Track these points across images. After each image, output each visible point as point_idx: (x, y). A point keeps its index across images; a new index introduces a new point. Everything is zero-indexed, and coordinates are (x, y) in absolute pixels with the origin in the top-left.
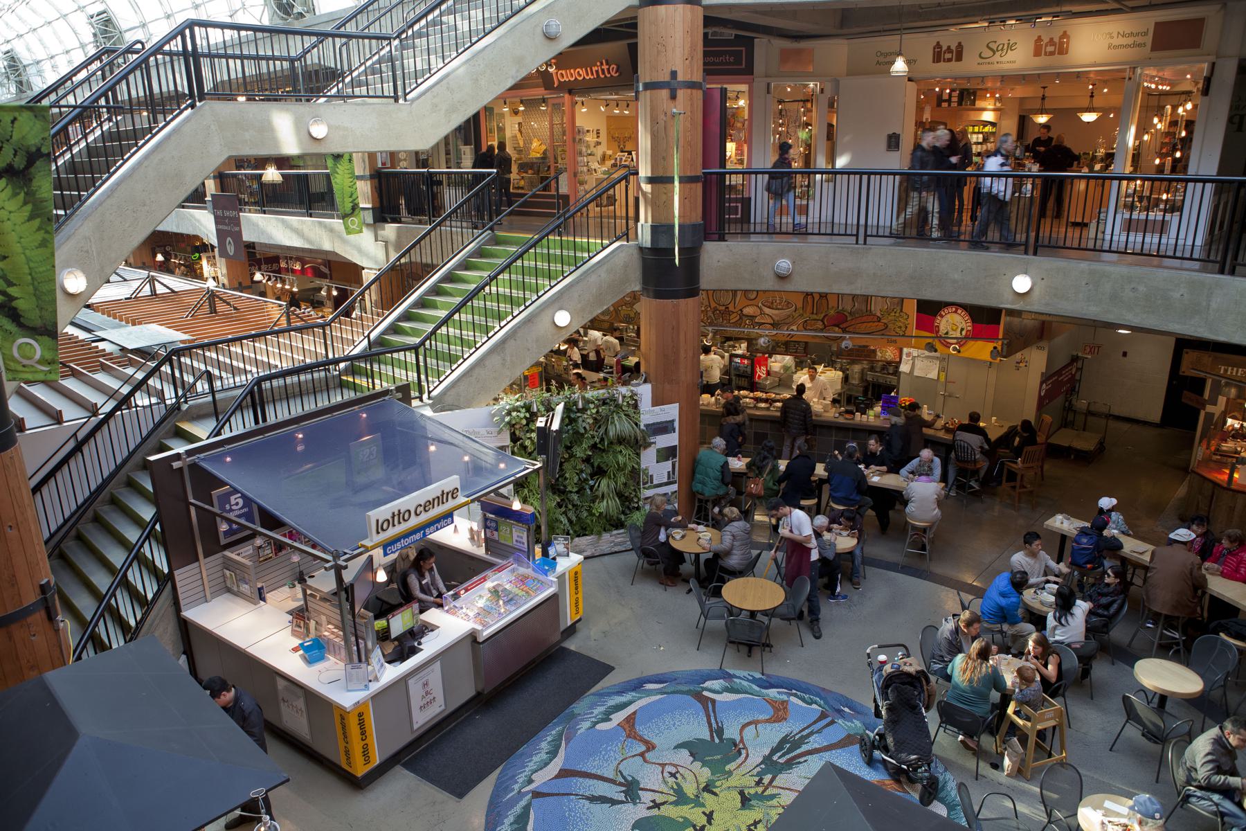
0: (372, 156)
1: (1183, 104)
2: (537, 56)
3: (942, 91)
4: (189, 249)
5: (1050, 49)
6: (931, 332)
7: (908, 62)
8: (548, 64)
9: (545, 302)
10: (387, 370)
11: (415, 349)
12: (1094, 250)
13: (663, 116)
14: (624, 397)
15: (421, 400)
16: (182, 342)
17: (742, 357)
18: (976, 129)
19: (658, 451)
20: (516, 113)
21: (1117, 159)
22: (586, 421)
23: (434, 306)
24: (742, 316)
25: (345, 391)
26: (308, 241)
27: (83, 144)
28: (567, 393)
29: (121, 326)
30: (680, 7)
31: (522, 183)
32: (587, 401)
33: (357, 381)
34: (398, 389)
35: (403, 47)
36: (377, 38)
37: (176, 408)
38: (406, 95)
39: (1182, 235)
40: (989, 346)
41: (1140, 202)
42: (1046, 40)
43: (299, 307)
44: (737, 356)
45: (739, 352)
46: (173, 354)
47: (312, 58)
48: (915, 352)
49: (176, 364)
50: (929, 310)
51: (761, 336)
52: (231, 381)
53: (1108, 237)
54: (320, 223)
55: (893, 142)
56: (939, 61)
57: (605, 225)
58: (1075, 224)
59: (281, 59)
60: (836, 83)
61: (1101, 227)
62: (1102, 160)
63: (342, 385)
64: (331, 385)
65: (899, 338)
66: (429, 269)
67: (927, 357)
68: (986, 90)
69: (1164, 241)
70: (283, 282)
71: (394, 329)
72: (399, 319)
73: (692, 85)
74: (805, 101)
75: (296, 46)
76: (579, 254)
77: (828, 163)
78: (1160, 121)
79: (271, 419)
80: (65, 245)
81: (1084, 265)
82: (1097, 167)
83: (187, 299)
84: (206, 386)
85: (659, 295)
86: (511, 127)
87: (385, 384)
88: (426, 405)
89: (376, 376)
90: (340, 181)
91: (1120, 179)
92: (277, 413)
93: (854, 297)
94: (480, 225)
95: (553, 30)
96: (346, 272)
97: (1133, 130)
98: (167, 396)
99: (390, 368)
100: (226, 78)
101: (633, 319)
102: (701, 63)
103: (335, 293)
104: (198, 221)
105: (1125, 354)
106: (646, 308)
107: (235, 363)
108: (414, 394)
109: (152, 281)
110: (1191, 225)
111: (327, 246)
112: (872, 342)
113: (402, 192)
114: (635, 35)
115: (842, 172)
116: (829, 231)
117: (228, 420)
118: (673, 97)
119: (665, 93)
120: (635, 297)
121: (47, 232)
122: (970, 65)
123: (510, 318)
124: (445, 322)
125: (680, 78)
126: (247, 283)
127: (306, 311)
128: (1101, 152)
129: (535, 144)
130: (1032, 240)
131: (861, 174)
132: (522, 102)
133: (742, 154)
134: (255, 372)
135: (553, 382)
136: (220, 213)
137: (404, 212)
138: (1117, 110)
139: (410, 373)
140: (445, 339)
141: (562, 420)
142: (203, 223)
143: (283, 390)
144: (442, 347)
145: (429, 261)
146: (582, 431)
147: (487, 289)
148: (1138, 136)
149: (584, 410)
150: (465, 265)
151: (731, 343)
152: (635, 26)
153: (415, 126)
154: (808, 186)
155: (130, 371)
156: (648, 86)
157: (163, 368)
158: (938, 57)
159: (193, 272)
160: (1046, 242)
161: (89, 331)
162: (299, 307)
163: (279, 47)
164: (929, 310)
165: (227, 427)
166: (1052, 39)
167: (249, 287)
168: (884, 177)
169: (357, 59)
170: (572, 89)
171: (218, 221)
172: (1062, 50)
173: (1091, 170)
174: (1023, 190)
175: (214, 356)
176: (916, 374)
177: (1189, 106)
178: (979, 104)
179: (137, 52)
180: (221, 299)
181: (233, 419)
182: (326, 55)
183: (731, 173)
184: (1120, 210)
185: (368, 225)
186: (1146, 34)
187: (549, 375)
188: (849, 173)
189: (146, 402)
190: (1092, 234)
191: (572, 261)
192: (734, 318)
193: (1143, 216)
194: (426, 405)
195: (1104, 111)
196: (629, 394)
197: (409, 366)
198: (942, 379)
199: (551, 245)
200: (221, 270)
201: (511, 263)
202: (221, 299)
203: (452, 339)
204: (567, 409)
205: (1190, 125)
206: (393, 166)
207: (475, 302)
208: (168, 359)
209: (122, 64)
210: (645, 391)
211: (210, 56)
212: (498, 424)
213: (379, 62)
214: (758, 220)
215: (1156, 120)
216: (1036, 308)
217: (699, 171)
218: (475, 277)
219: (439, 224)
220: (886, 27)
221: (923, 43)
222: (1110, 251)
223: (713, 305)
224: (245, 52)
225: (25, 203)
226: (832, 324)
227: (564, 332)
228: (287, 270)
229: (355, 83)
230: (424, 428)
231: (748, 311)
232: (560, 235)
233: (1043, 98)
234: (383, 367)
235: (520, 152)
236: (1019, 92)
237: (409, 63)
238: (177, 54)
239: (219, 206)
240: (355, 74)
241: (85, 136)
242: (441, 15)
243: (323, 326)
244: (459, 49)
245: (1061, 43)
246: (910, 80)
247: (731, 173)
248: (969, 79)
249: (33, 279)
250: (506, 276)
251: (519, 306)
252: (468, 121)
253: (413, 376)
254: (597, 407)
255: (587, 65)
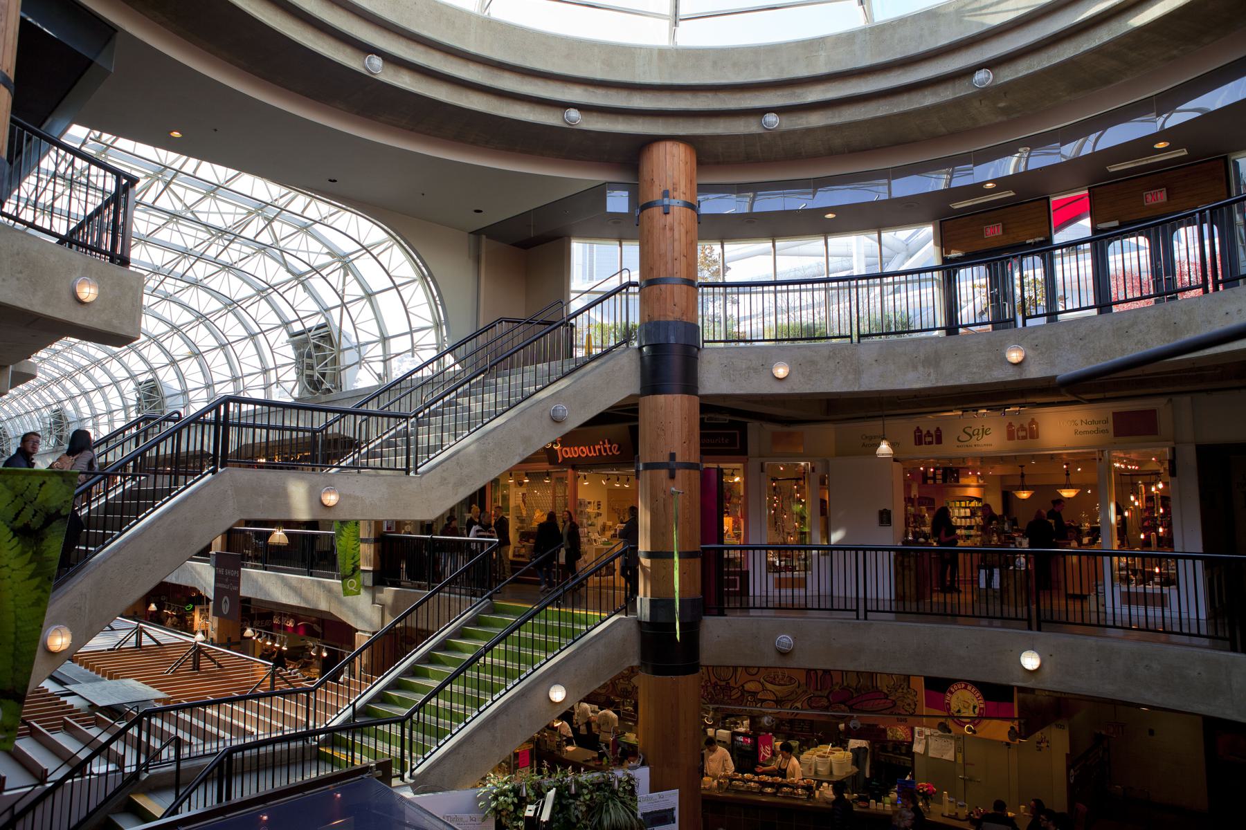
0: (378, 523)
1: (1155, 483)
2: (546, 437)
3: (926, 469)
4: (184, 599)
5: (1022, 434)
6: (942, 709)
7: (892, 445)
8: (555, 443)
9: (541, 675)
10: (369, 742)
11: (401, 721)
12: (1098, 625)
13: (662, 495)
14: (620, 781)
15: (402, 779)
16: (157, 700)
17: (745, 735)
18: (963, 504)
20: (521, 484)
21: (1103, 532)
22: (578, 809)
23: (425, 675)
24: (743, 691)
25: (322, 765)
26: (305, 600)
27: (103, 501)
28: (559, 776)
29: (96, 680)
30: (678, 397)
31: (523, 551)
32: (580, 786)
33: (336, 754)
34: (379, 766)
35: (419, 423)
36: (396, 417)
37: (135, 776)
38: (417, 468)
39: (1184, 609)
40: (1007, 726)
41: (1135, 575)
42: (1016, 426)
43: (285, 667)
44: (740, 734)
45: (742, 730)
46: (142, 716)
47: (334, 429)
48: (927, 732)
49: (145, 725)
50: (938, 686)
51: (765, 714)
52: (201, 748)
53: (1110, 610)
54: (319, 582)
55: (885, 518)
56: (920, 443)
57: (604, 596)
58: (1074, 597)
59: (304, 430)
60: (827, 464)
61: (1101, 600)
62: (1088, 534)
63: (320, 758)
64: (308, 757)
65: (910, 717)
66: (425, 635)
67: (940, 736)
68: (968, 468)
69: (1167, 614)
70: (273, 639)
71: (381, 698)
72: (388, 687)
73: (689, 466)
74: (798, 479)
75: (319, 420)
76: (577, 627)
77: (823, 537)
78: (1137, 499)
79: (236, 797)
80: (60, 602)
81: (1091, 641)
82: (1086, 540)
83: (171, 653)
84: (172, 753)
85: (657, 671)
86: (515, 497)
87: (365, 759)
88: (408, 784)
89: (357, 748)
90: (344, 544)
91: (1111, 555)
92: (245, 789)
93: (859, 674)
94: (479, 593)
95: (560, 413)
96: (336, 632)
97: (1113, 507)
98: (127, 762)
99: (372, 740)
100: (250, 441)
101: (630, 694)
102: (698, 446)
103: (325, 654)
104: (199, 574)
105: (1151, 732)
106: (645, 683)
107: (208, 727)
108: (396, 771)
109: (139, 632)
110: (1190, 599)
111: (323, 606)
112: (880, 721)
113: (403, 556)
114: (636, 419)
115: (837, 548)
116: (829, 606)
117: (189, 796)
118: (672, 477)
119: (664, 473)
120: (632, 670)
121: (45, 591)
122: (950, 448)
123: (503, 691)
124: (436, 693)
125: (679, 459)
126: (236, 638)
127: (292, 671)
128: (1086, 526)
129: (538, 514)
130: (1034, 614)
131: (857, 550)
132: (527, 475)
133: (739, 529)
134: (229, 740)
135: (545, 763)
136: (221, 571)
137: (404, 576)
138: (1094, 487)
139: (393, 747)
140: (434, 711)
141: (554, 806)
142: (204, 576)
143: (254, 761)
144: (430, 719)
145: (425, 627)
146: (574, 820)
147: (481, 660)
148: (1119, 511)
149: (576, 796)
150: (461, 633)
151: (733, 719)
152: (636, 411)
153: (424, 499)
154: (805, 559)
155: (93, 732)
156: (648, 466)
157: (130, 731)
158: (919, 440)
159: (184, 625)
160: (1048, 617)
161: (62, 683)
162: (285, 667)
163: (304, 420)
164: (938, 686)
165: (185, 805)
166: (1022, 426)
167: (238, 643)
168: (879, 553)
169: (374, 431)
170: (576, 465)
171: (218, 578)
172: (1034, 435)
173: (1080, 544)
174: (1017, 563)
175: (188, 718)
176: (931, 754)
177: (1160, 486)
178: (963, 481)
179: (175, 421)
180: (206, 655)
181: (194, 795)
182: (348, 428)
183: (728, 549)
184: (1117, 583)
185: (366, 588)
186: (1107, 422)
187: (542, 753)
188: (845, 549)
189: (103, 769)
190: (1093, 607)
191: (570, 633)
192: (736, 694)
193: (1140, 588)
194: (408, 784)
195: (1082, 487)
196: (625, 778)
197: (393, 739)
198: (960, 760)
199: (549, 616)
200: (213, 623)
201: (508, 634)
202: (206, 655)
203: (441, 712)
204: (559, 796)
205: (1165, 500)
206: (398, 531)
207: (468, 672)
208: (137, 722)
209: (155, 434)
210: (642, 775)
211: (240, 426)
212: (483, 810)
213: (395, 436)
214: (758, 593)
215: (1132, 498)
216: (1049, 685)
217: (698, 547)
218: (470, 645)
219: (439, 590)
220: (869, 414)
221: (905, 427)
222: (1114, 627)
223: (713, 680)
224: (272, 423)
225: (30, 562)
226: (838, 701)
227: (558, 708)
228: (279, 627)
229: (371, 454)
230: (402, 813)
231: (750, 686)
232: (559, 606)
233: (1023, 476)
234: (365, 739)
235: (522, 521)
236: (998, 470)
237: (423, 438)
238: (210, 423)
239: (220, 562)
240: (371, 446)
241: (106, 494)
242: (457, 396)
243: (308, 691)
244: (471, 424)
245: (1031, 429)
246: (895, 460)
247: (728, 549)
248: (950, 460)
249: (17, 638)
250: (502, 646)
251: (514, 679)
252: (475, 494)
253: (396, 750)
254: (591, 792)
255: (590, 443)
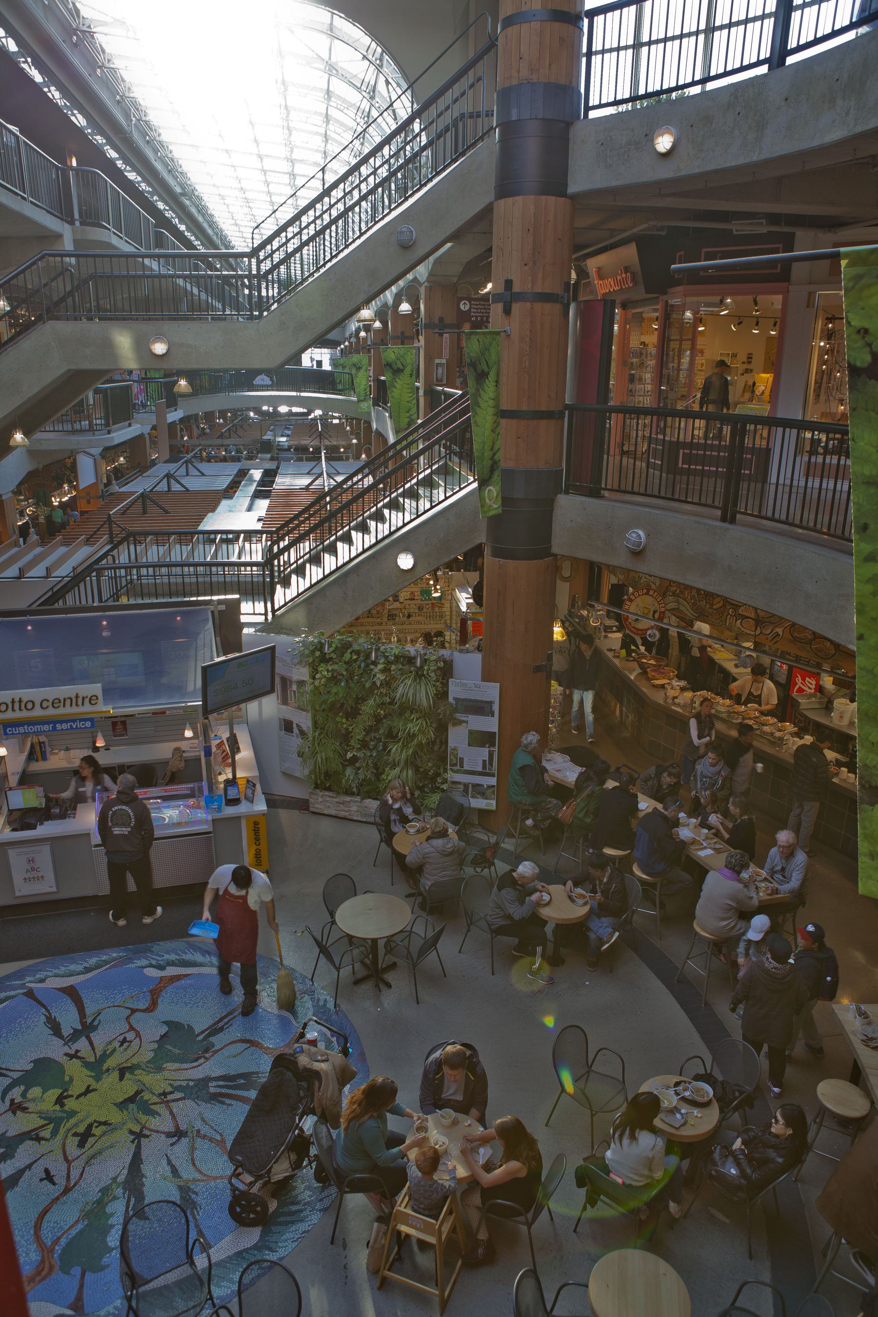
19: (471, 732)
